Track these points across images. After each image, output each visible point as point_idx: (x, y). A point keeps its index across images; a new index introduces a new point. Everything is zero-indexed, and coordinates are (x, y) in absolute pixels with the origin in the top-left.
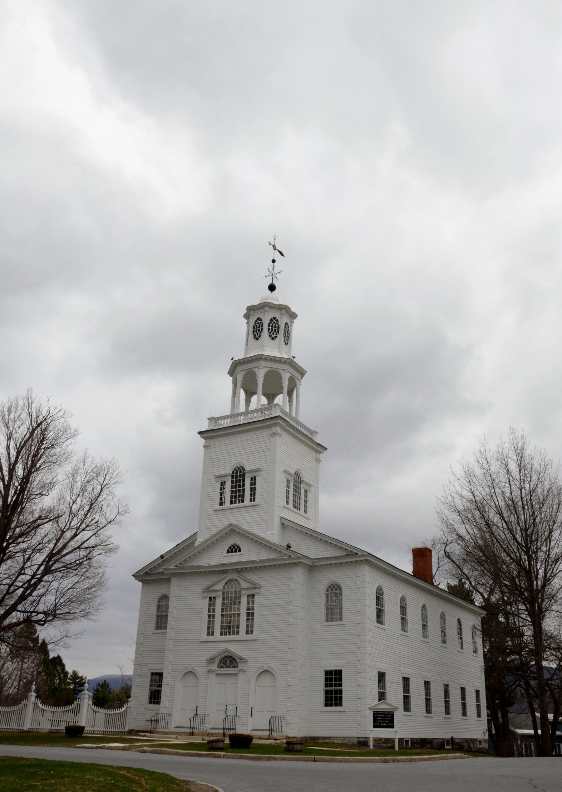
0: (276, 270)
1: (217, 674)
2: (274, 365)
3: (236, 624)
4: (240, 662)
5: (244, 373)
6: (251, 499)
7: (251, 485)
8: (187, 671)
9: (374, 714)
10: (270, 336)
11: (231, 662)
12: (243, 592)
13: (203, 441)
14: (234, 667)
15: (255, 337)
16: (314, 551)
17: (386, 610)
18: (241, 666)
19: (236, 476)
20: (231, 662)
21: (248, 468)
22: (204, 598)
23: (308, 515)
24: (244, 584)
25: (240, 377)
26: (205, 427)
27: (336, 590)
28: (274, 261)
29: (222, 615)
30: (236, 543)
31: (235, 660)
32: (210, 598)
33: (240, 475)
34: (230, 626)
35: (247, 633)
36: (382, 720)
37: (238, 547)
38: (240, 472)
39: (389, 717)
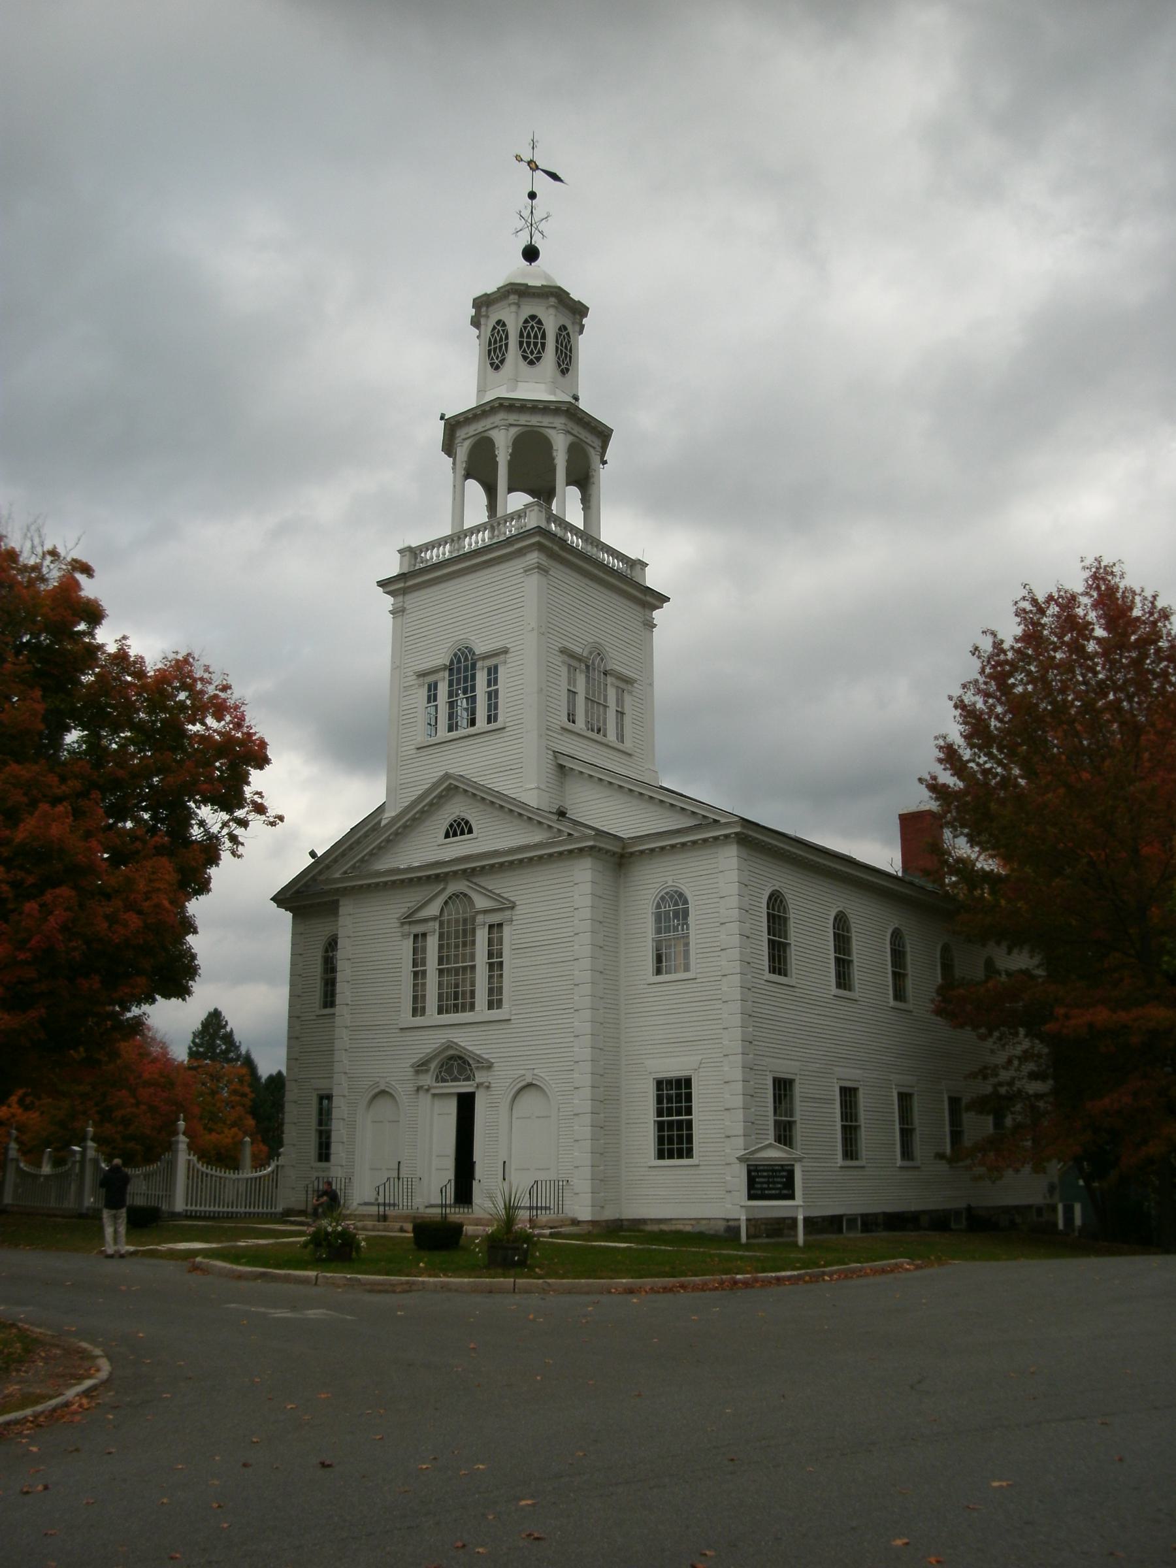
0: (538, 215)
1: (434, 1095)
2: (534, 420)
3: (469, 988)
4: (477, 1068)
5: (470, 444)
6: (489, 717)
7: (489, 685)
8: (377, 1090)
9: (749, 1172)
10: (525, 358)
11: (462, 1070)
12: (480, 919)
13: (390, 599)
14: (468, 1079)
15: (492, 364)
16: (625, 820)
17: (793, 943)
18: (480, 1077)
19: (459, 669)
20: (462, 1070)
21: (480, 649)
22: (405, 936)
23: (628, 745)
25: (462, 451)
26: (393, 570)
27: (676, 904)
28: (532, 196)
29: (441, 971)
30: (463, 815)
31: (469, 1065)
32: (416, 936)
33: (466, 668)
34: (456, 994)
35: (490, 1006)
36: (768, 1183)
37: (467, 822)
38: (466, 659)
39: (782, 1177)
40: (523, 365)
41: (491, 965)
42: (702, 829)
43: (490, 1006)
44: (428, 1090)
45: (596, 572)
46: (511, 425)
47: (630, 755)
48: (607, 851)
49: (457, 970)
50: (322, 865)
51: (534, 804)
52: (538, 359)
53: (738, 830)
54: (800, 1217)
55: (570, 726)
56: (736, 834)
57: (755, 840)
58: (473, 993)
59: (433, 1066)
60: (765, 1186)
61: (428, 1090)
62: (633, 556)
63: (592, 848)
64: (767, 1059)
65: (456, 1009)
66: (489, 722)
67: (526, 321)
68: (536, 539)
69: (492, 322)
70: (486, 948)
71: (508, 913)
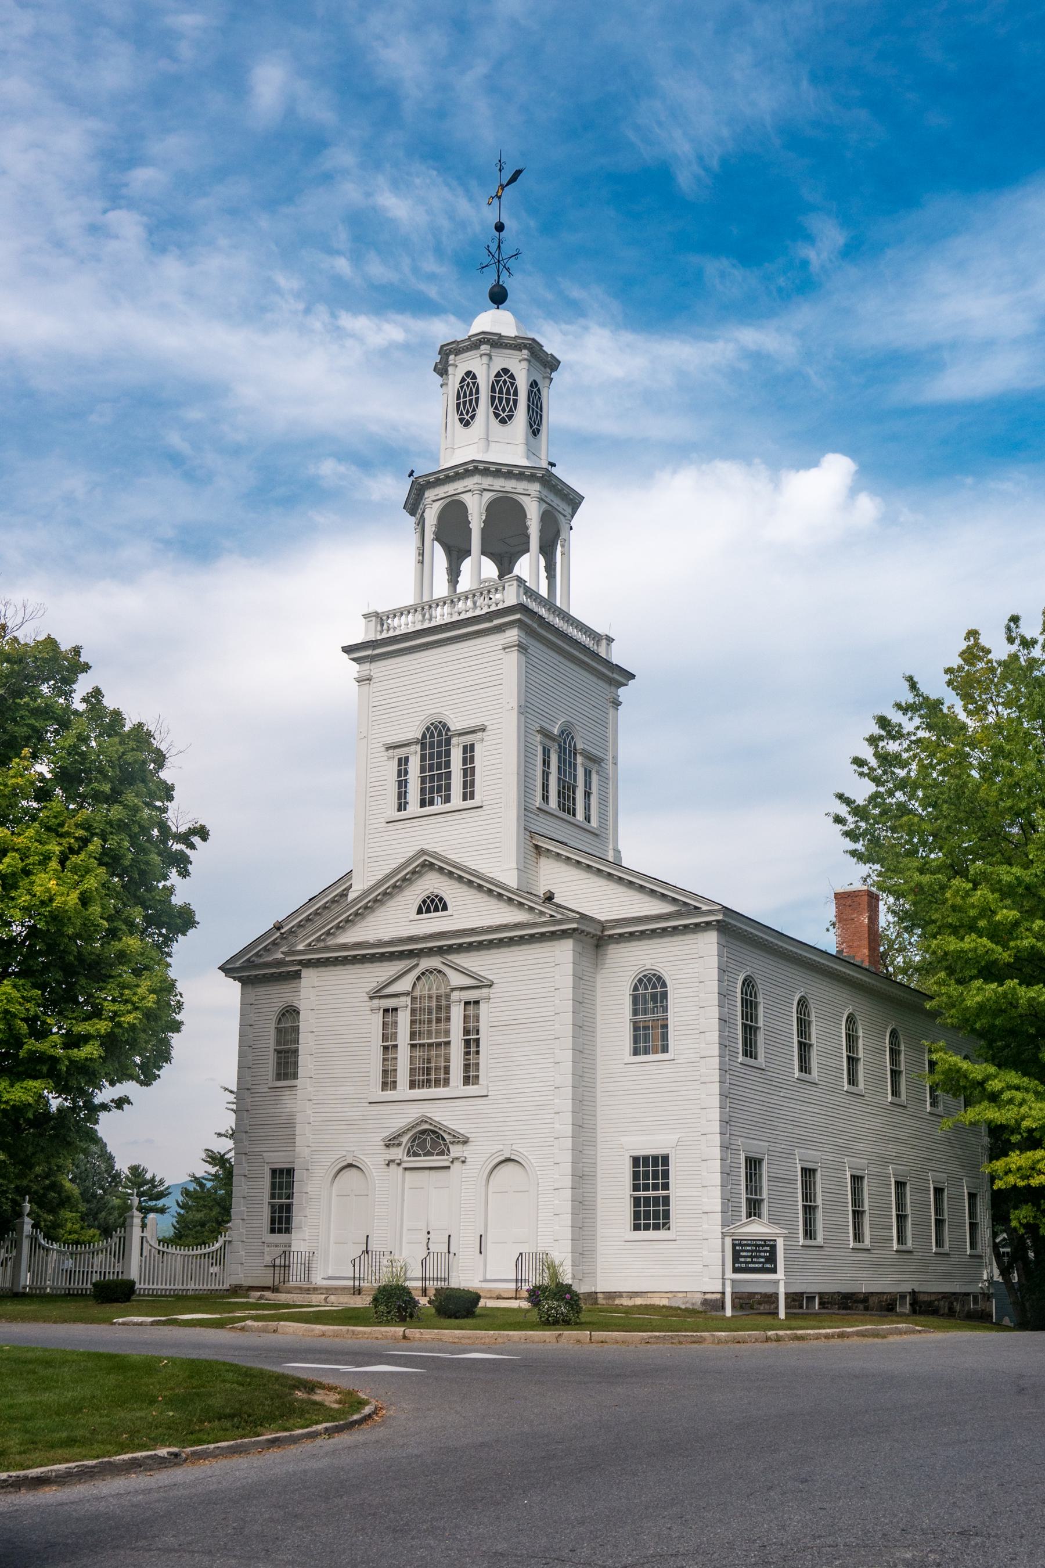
1: (406, 1169)
2: (509, 485)
3: (443, 1064)
4: (452, 1143)
10: (497, 415)
11: (435, 1144)
12: (455, 995)
14: (442, 1153)
18: (455, 1151)
20: (435, 1144)
24: (456, 979)
27: (654, 987)
30: (437, 892)
31: (444, 1139)
33: (440, 743)
35: (467, 1081)
36: (751, 1257)
37: (441, 899)
38: (440, 734)
39: (766, 1251)
40: (494, 422)
41: (467, 1043)
42: (684, 915)
43: (467, 1081)
44: (399, 1164)
45: (586, 659)
46: (485, 490)
47: (596, 835)
48: (588, 933)
49: (430, 1045)
50: (281, 933)
51: (513, 884)
52: (510, 417)
53: (720, 917)
54: (782, 1291)
55: (544, 807)
56: (718, 921)
57: (736, 930)
58: (447, 1069)
59: (405, 1139)
60: (749, 1260)
61: (399, 1164)
62: (600, 629)
63: (574, 930)
64: (741, 1139)
65: (427, 1083)
66: (465, 799)
67: (498, 375)
68: (518, 616)
69: (460, 373)
70: (462, 1025)
71: (485, 990)
